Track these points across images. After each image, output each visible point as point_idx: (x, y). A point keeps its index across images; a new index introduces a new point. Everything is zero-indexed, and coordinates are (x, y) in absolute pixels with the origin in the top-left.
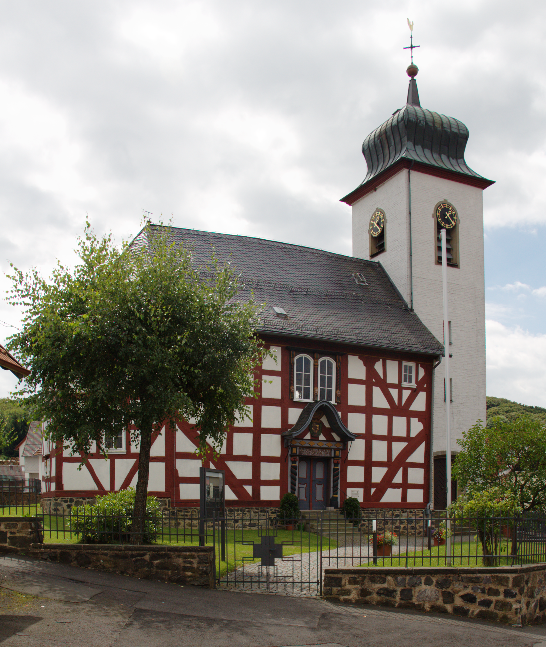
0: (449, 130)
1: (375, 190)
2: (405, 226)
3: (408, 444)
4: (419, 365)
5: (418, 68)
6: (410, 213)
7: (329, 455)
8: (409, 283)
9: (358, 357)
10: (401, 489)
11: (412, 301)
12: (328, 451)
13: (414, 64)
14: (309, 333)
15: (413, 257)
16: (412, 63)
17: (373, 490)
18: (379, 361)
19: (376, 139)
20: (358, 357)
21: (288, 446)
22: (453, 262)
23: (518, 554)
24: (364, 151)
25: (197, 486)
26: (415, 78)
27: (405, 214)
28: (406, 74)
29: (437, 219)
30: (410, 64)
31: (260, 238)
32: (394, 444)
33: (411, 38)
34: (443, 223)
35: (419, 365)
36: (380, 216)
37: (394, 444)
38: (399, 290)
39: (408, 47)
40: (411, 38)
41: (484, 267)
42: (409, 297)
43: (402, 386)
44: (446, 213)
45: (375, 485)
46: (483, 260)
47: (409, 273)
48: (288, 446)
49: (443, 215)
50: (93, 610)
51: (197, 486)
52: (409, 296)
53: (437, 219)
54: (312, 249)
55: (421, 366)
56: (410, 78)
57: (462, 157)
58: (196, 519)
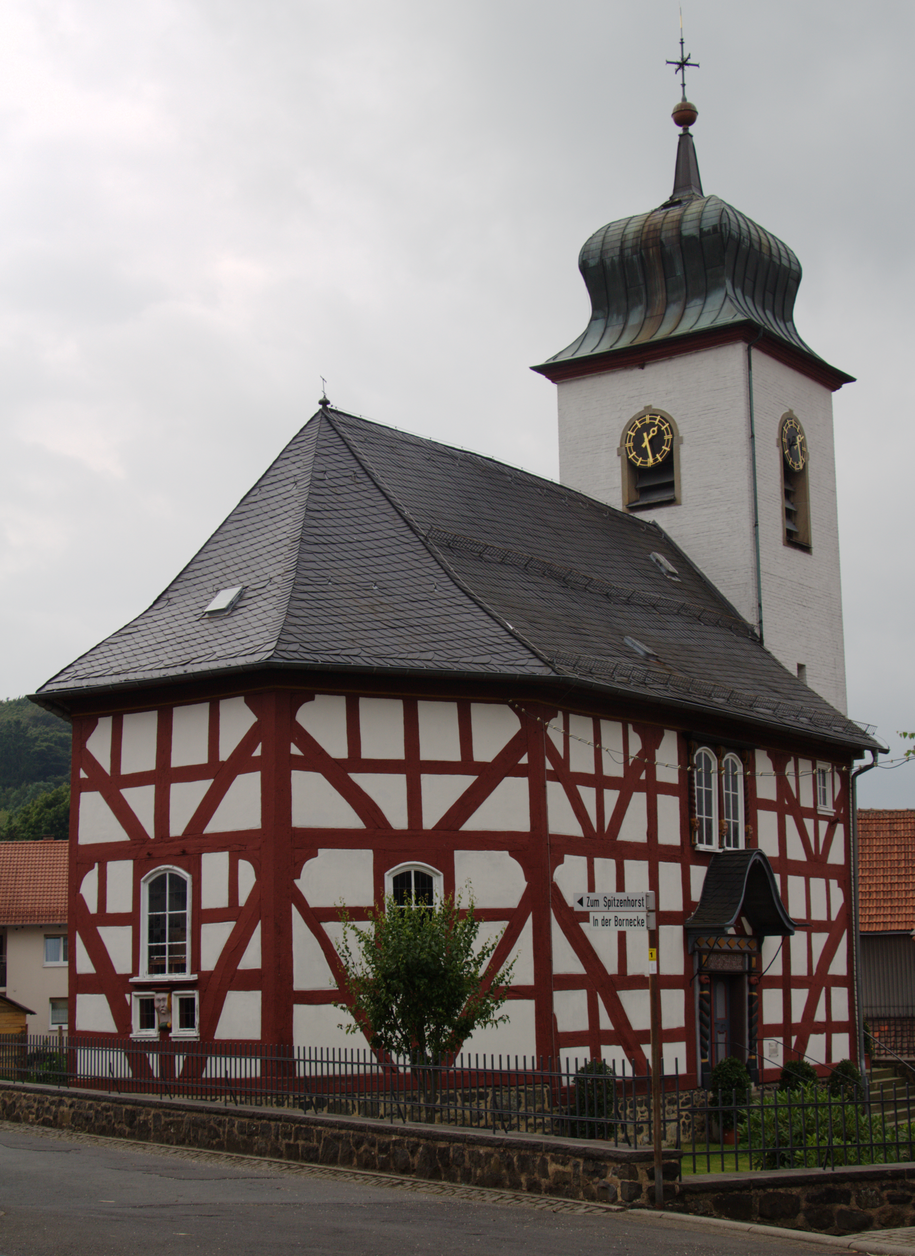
0: (778, 262)
1: (642, 367)
2: (745, 462)
4: (630, 727)
5: (698, 110)
6: (753, 436)
7: (739, 968)
8: (752, 583)
10: (825, 1034)
11: (761, 622)
12: (739, 959)
13: (689, 100)
14: (617, 684)
15: (761, 528)
16: (684, 99)
18: (556, 716)
19: (628, 252)
21: (694, 951)
22: (800, 539)
23: (204, 1076)
24: (584, 268)
25: (112, 866)
26: (692, 129)
27: (744, 436)
28: (671, 121)
30: (679, 101)
31: (496, 459)
33: (682, 43)
35: (630, 727)
36: (659, 428)
38: (725, 595)
40: (682, 43)
41: (838, 552)
42: (755, 614)
43: (819, 813)
46: (837, 538)
47: (753, 562)
48: (694, 951)
52: (755, 610)
54: (570, 490)
55: (635, 730)
56: (680, 130)
57: (791, 320)
58: (898, 1153)
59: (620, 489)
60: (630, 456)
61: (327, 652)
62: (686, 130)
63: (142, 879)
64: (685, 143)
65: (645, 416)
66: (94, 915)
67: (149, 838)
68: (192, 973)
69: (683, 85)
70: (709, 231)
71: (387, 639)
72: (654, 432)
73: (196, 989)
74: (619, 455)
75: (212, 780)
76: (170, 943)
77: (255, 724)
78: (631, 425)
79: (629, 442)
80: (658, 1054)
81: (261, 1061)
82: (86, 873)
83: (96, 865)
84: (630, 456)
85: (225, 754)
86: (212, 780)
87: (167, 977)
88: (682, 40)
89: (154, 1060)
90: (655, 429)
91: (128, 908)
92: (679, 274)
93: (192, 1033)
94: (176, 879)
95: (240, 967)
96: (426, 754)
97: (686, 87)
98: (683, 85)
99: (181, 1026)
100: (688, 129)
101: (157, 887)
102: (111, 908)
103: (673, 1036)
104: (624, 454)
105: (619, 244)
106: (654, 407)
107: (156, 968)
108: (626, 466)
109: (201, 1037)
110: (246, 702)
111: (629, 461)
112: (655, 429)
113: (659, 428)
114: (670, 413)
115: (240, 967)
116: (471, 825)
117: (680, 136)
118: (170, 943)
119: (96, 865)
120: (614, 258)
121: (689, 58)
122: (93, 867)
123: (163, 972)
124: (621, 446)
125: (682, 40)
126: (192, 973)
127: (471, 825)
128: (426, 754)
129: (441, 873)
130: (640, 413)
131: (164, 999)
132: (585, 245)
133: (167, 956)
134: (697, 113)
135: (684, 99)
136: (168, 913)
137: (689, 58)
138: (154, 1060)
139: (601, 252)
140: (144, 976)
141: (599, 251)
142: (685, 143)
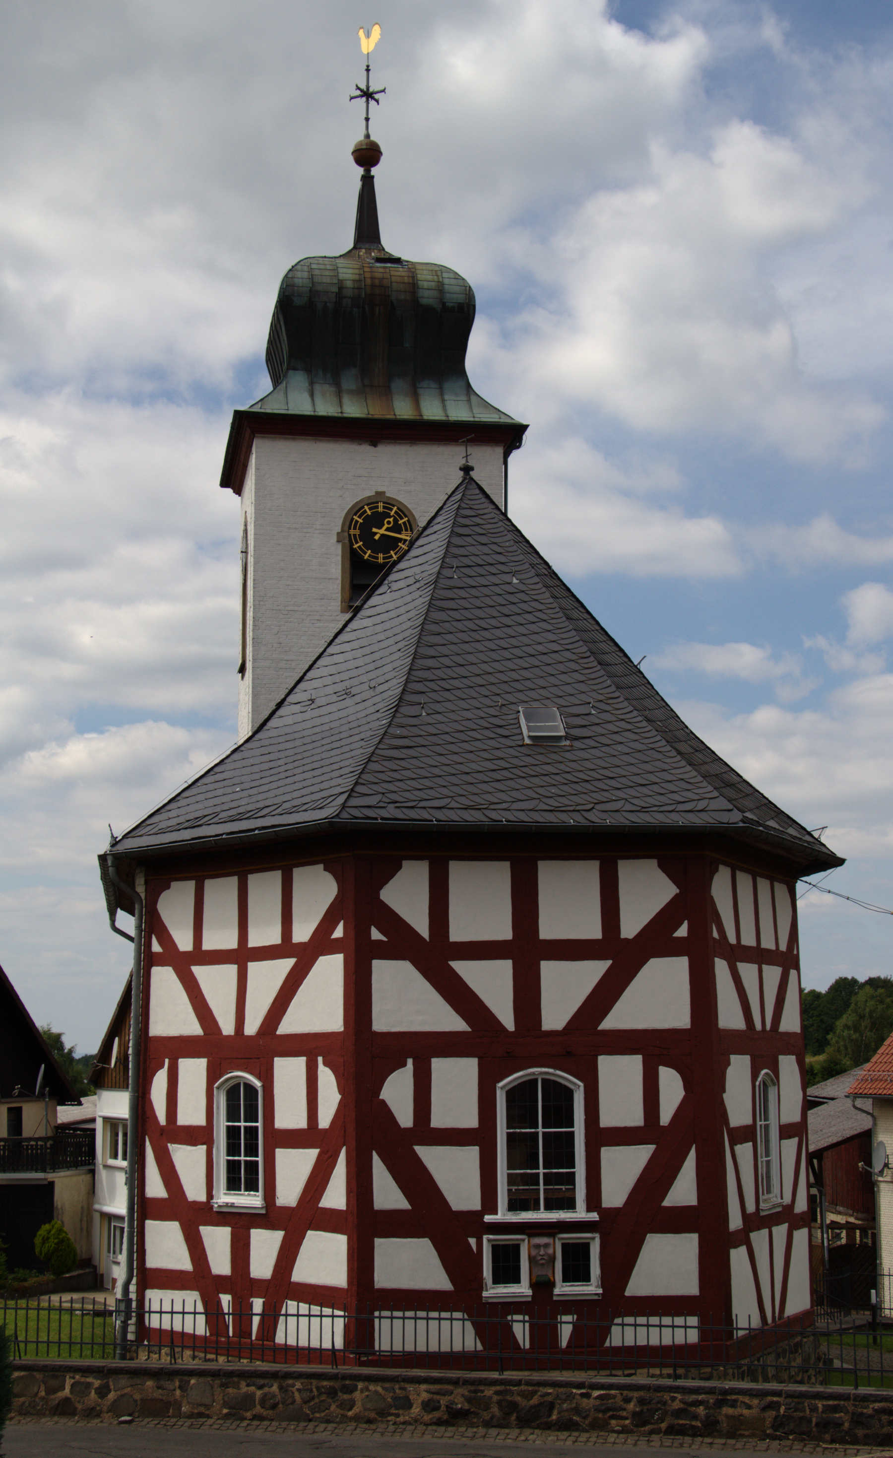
1: (374, 445)
3: (320, 1156)
5: (383, 150)
9: (321, 866)
13: (372, 138)
16: (368, 136)
17: (682, 931)
20: (321, 866)
25: (440, 1066)
26: (374, 171)
29: (351, 545)
30: (361, 137)
32: (549, 970)
34: (369, 552)
37: (549, 970)
39: (365, 105)
40: (368, 70)
44: (377, 537)
45: (672, 949)
49: (366, 535)
50: (635, 1429)
51: (440, 1066)
53: (351, 545)
56: (360, 171)
59: (339, 582)
60: (356, 546)
61: (662, 809)
62: (368, 171)
63: (216, 1085)
64: (368, 181)
65: (377, 502)
66: (406, 1130)
67: (504, 1029)
68: (589, 1210)
69: (367, 119)
70: (453, 307)
71: (572, 785)
72: (389, 523)
73: (596, 1232)
74: (338, 541)
75: (609, 962)
76: (545, 1171)
77: (677, 895)
78: (357, 509)
79: (355, 528)
80: (171, 1361)
81: (374, 1348)
82: (678, 1072)
83: (410, 1062)
84: (356, 546)
85: (630, 928)
86: (609, 962)
87: (542, 1216)
88: (368, 66)
89: (521, 1330)
90: (391, 520)
91: (470, 1120)
92: (407, 345)
93: (592, 1288)
94: (249, 1088)
95: (666, 1203)
96: (548, 930)
97: (370, 122)
98: (367, 119)
99: (564, 1281)
100: (370, 171)
101: (232, 1094)
102: (439, 1120)
103: (377, 1317)
104: (347, 541)
105: (335, 289)
106: (388, 495)
107: (515, 1205)
108: (348, 556)
109: (533, 1296)
110: (660, 866)
111: (353, 552)
112: (391, 520)
113: (396, 521)
114: (409, 506)
115: (666, 1203)
116: (610, 1023)
117: (363, 177)
118: (545, 1171)
119: (410, 1062)
120: (328, 304)
121: (358, 88)
122: (404, 1065)
123: (536, 1208)
124: (343, 531)
125: (368, 66)
126: (589, 1210)
127: (610, 1023)
128: (548, 930)
129: (581, 1084)
130: (369, 497)
131: (546, 1246)
132: (286, 276)
133: (542, 1187)
134: (381, 153)
135: (368, 136)
136: (540, 1130)
137: (358, 88)
138: (521, 1330)
139: (311, 291)
140: (502, 1215)
141: (309, 289)
142: (368, 181)
